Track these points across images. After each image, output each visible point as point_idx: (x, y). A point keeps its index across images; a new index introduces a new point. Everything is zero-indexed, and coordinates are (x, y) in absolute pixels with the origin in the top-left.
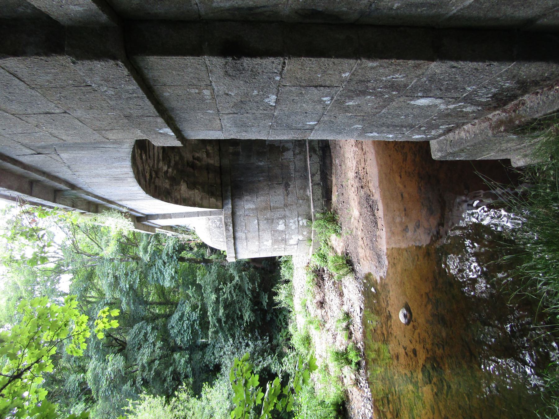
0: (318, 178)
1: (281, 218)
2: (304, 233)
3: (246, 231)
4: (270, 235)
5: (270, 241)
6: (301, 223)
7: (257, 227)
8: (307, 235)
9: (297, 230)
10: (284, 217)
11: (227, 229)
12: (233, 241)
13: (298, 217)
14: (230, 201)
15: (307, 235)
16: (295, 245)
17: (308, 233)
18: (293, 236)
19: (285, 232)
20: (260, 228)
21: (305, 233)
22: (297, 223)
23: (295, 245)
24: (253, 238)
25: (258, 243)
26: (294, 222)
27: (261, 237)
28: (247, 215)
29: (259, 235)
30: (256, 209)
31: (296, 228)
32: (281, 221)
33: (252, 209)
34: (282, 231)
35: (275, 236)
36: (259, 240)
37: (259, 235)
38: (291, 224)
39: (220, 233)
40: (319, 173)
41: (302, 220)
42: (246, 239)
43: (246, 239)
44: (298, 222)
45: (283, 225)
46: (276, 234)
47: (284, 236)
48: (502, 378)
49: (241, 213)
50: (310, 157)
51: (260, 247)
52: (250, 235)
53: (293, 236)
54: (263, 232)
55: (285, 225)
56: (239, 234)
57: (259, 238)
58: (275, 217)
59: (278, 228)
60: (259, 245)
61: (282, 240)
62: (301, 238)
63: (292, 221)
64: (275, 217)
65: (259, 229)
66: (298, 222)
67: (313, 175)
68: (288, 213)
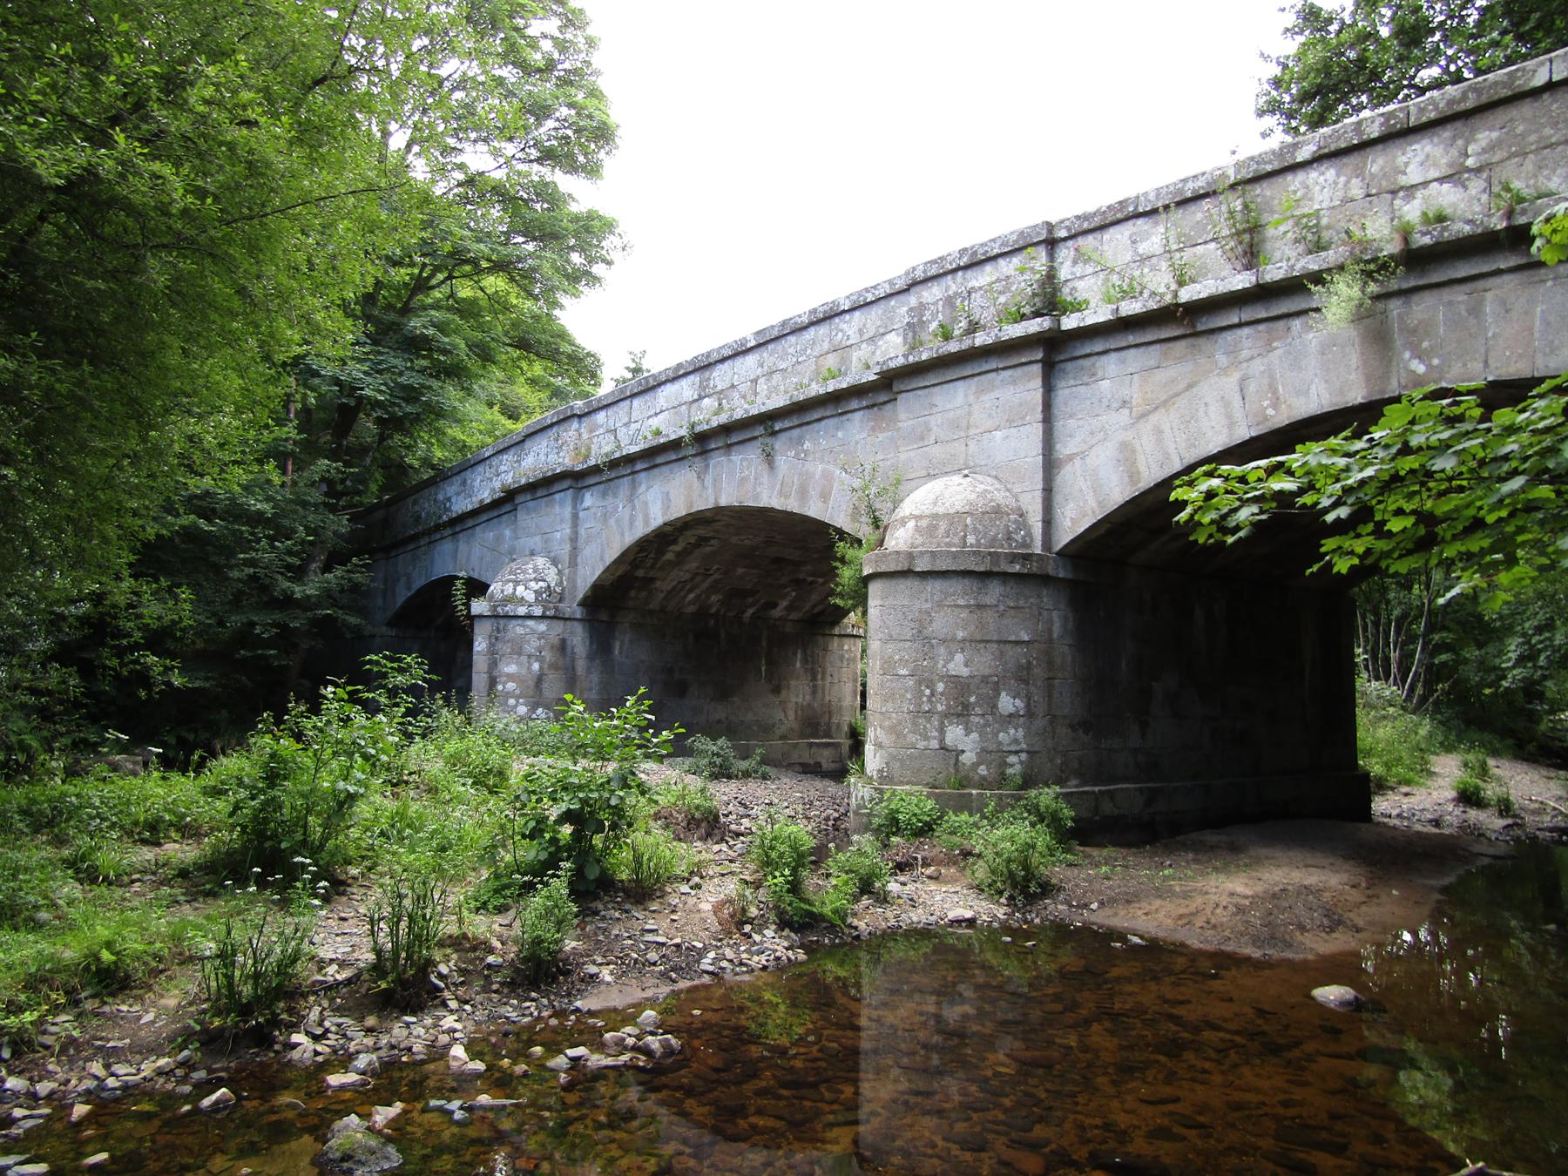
0: (1107, 808)
1: (1028, 705)
2: (983, 767)
3: (1002, 608)
4: (987, 672)
5: (965, 672)
6: (1012, 759)
7: (1013, 638)
8: (976, 777)
9: (993, 747)
10: (1030, 714)
11: (1013, 558)
12: (982, 569)
13: (1028, 752)
14: (1070, 576)
15: (976, 777)
16: (942, 740)
17: (984, 778)
18: (975, 736)
19: (993, 714)
20: (1008, 647)
21: (983, 770)
22: (1013, 748)
23: (942, 740)
24: (981, 625)
25: (959, 638)
26: (1016, 741)
27: (982, 645)
28: (1040, 614)
29: (988, 641)
30: (1051, 641)
31: (1000, 743)
32: (1022, 705)
33: (1050, 631)
34: (995, 706)
35: (982, 685)
36: (971, 641)
37: (988, 641)
38: (1012, 731)
39: (994, 539)
40: (1116, 812)
41: (1021, 763)
42: (980, 607)
43: (980, 607)
44: (1016, 752)
45: (1011, 709)
46: (987, 690)
47: (978, 710)
48: (1407, 937)
49: (1045, 600)
50: (1140, 790)
51: (944, 641)
52: (989, 616)
53: (975, 736)
54: (997, 653)
55: (1011, 715)
56: (994, 592)
57: (981, 641)
58: (1032, 689)
59: (1003, 694)
60: (954, 639)
61: (966, 706)
62: (968, 758)
63: (1021, 733)
64: (1032, 689)
65: (1006, 642)
66: (1016, 752)
67: (1111, 794)
68: (1040, 723)
